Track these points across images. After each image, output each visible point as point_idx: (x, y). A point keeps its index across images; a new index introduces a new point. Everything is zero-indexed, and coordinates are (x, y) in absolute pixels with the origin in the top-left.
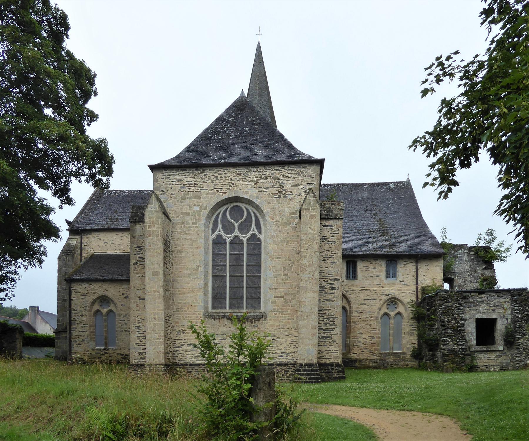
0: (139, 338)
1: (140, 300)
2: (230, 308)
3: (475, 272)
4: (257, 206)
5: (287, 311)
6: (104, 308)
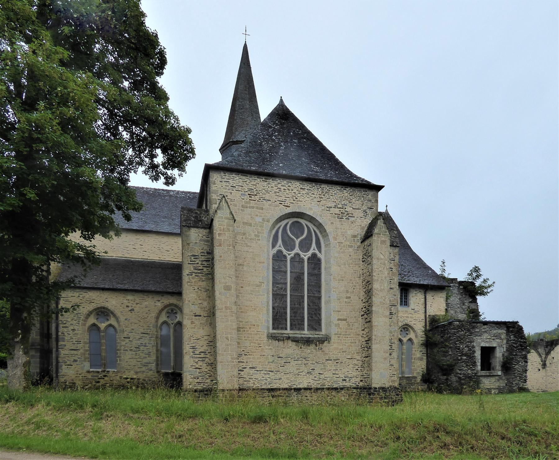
0: (195, 359)
1: (196, 316)
2: (291, 329)
3: (464, 304)
4: (321, 224)
5: (350, 334)
6: (101, 323)
